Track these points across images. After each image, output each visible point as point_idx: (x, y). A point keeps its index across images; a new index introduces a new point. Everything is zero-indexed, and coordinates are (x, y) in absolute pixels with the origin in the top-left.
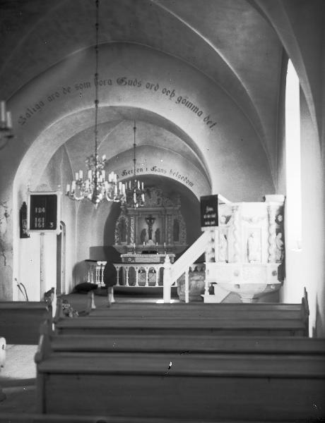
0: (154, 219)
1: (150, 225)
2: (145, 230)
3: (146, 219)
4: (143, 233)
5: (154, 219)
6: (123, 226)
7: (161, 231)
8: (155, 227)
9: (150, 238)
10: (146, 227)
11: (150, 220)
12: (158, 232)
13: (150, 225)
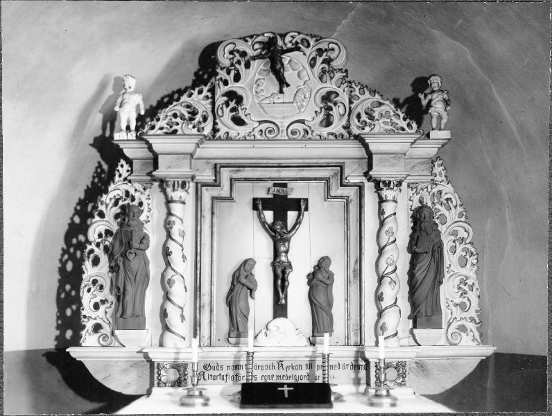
0: (299, 205)
1: (279, 236)
2: (247, 265)
3: (258, 205)
4: (241, 281)
5: (299, 205)
6: (126, 243)
7: (337, 269)
8: (312, 240)
9: (280, 310)
10: (254, 244)
11: (280, 209)
12: (319, 278)
13: (279, 236)
